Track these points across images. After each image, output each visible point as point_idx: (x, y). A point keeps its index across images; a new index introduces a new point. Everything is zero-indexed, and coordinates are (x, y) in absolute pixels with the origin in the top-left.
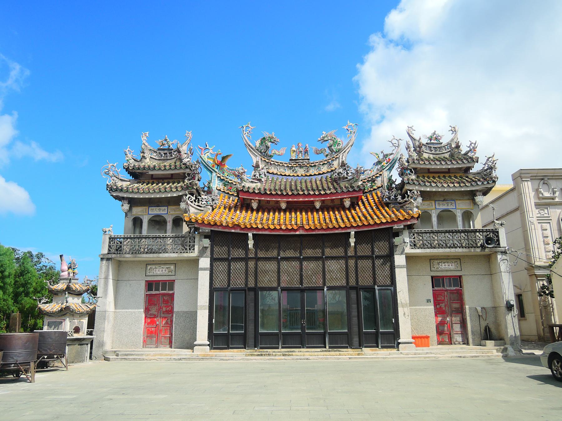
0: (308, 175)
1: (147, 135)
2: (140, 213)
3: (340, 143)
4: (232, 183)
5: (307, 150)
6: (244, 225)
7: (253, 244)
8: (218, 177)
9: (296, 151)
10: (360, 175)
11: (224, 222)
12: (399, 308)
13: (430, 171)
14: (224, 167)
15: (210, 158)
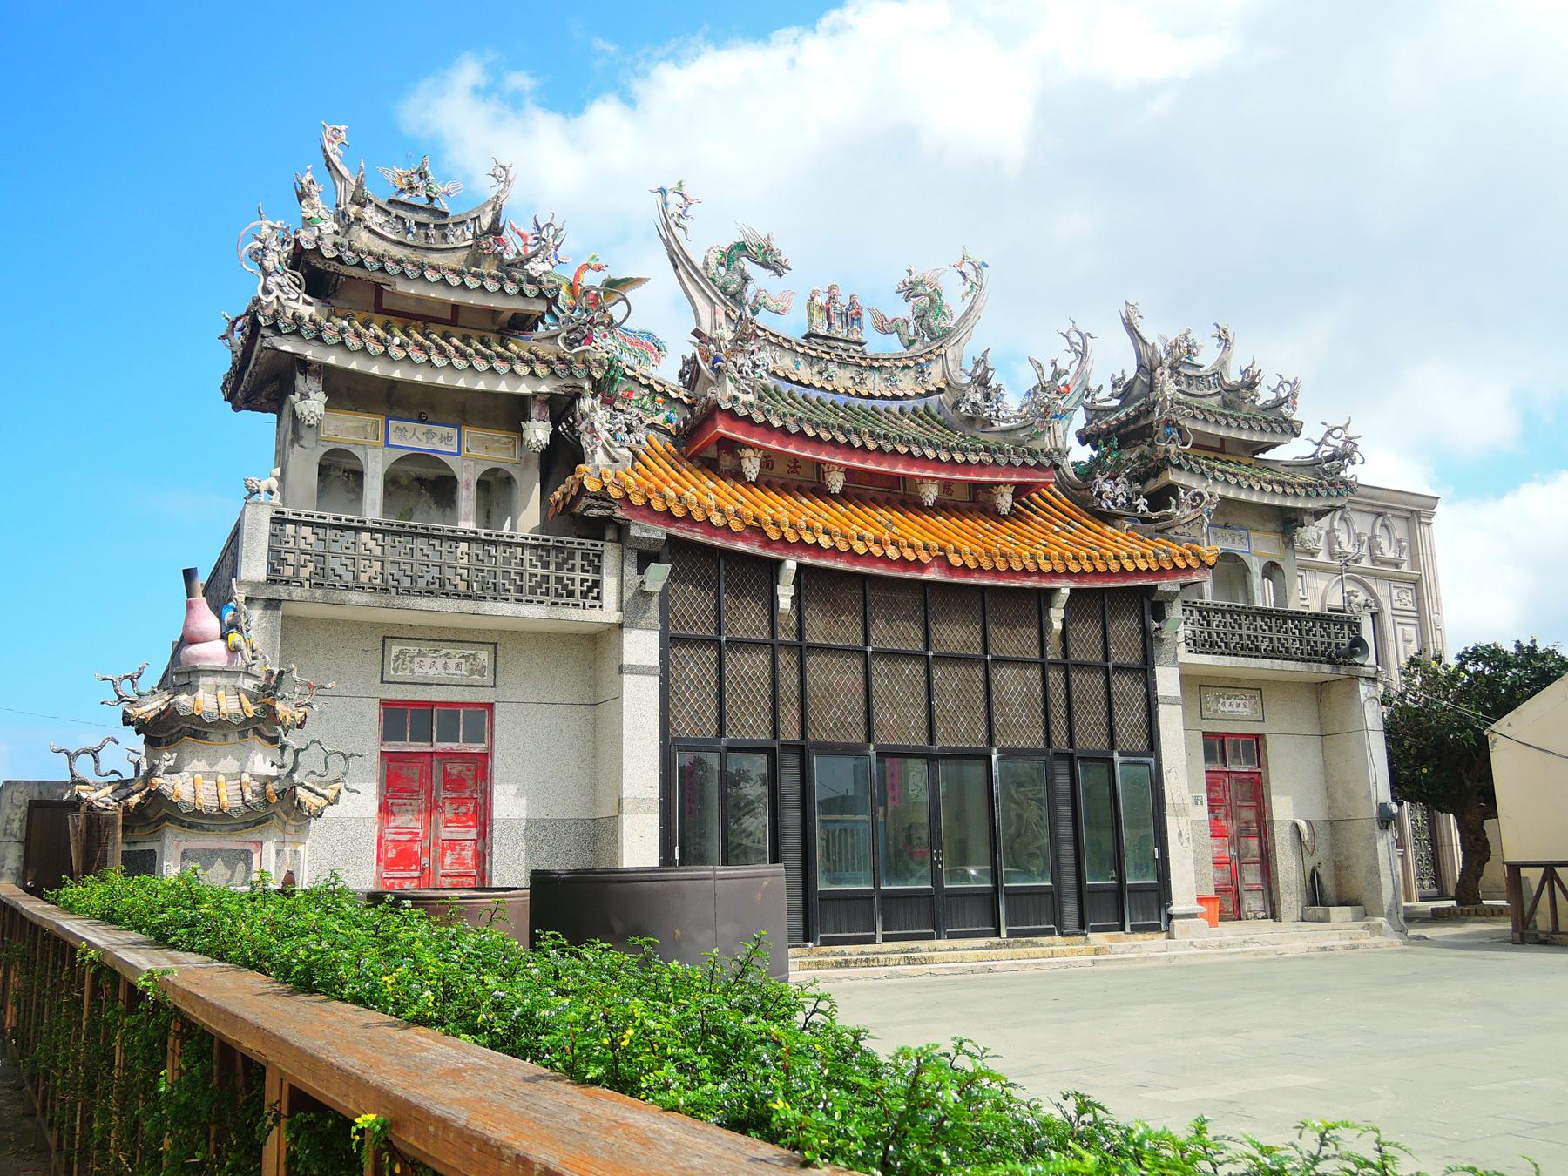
1: (343, 136)
2: (352, 437)
4: (634, 379)
12: (1168, 818)
13: (384, 307)
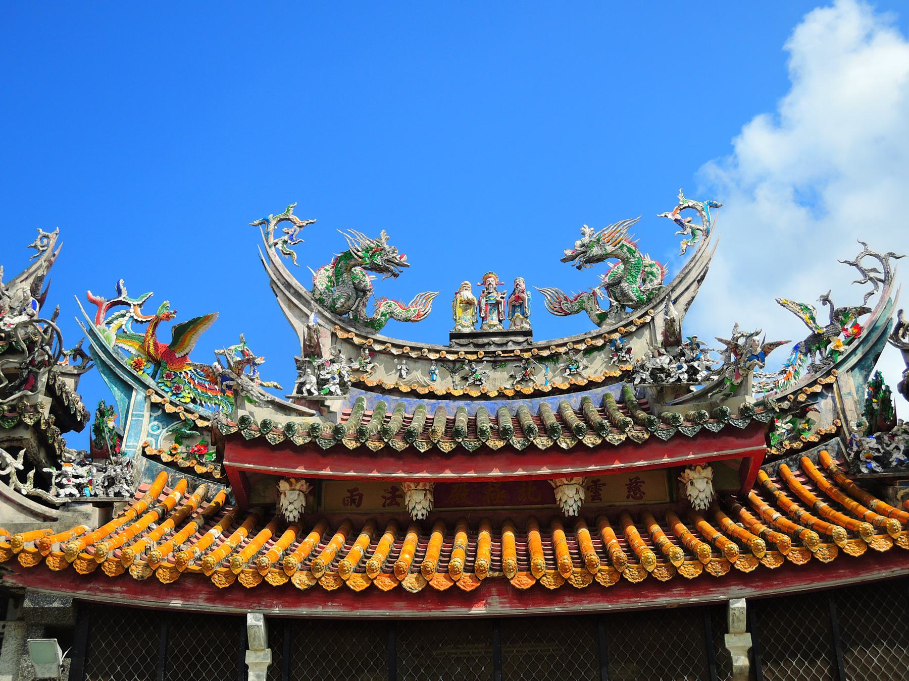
0: (528, 390)
3: (654, 270)
5: (518, 298)
6: (229, 575)
7: (269, 668)
8: (155, 406)
9: (476, 302)
10: (748, 364)
11: (138, 561)
14: (182, 368)
15: (131, 338)
